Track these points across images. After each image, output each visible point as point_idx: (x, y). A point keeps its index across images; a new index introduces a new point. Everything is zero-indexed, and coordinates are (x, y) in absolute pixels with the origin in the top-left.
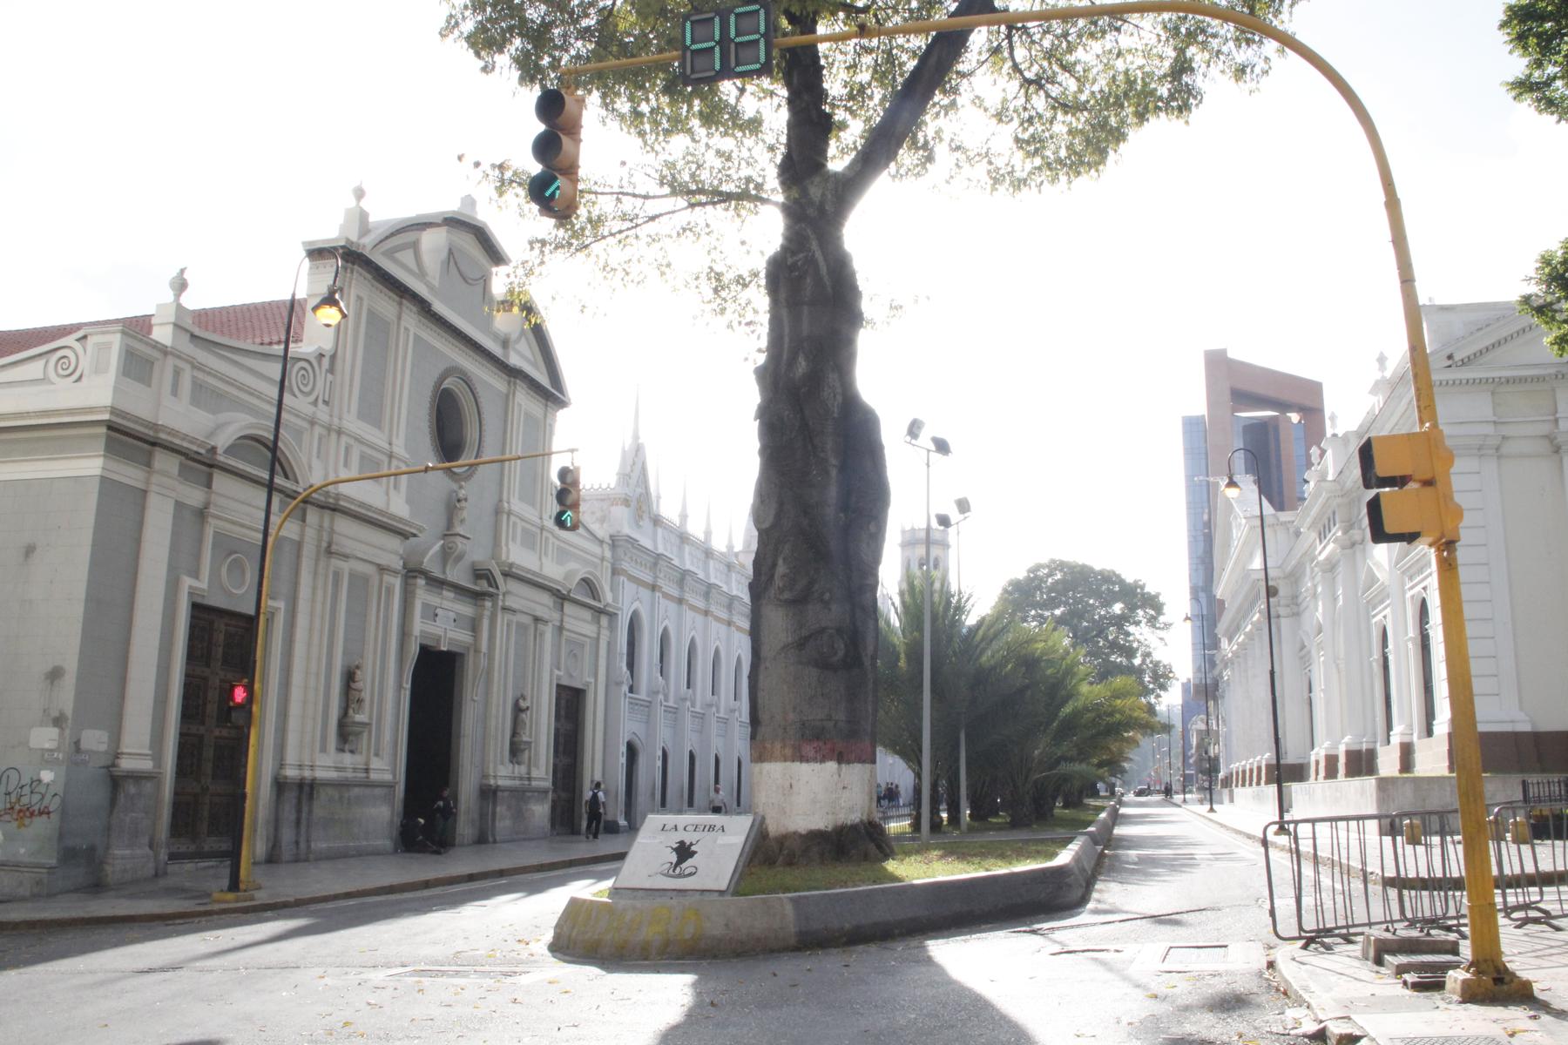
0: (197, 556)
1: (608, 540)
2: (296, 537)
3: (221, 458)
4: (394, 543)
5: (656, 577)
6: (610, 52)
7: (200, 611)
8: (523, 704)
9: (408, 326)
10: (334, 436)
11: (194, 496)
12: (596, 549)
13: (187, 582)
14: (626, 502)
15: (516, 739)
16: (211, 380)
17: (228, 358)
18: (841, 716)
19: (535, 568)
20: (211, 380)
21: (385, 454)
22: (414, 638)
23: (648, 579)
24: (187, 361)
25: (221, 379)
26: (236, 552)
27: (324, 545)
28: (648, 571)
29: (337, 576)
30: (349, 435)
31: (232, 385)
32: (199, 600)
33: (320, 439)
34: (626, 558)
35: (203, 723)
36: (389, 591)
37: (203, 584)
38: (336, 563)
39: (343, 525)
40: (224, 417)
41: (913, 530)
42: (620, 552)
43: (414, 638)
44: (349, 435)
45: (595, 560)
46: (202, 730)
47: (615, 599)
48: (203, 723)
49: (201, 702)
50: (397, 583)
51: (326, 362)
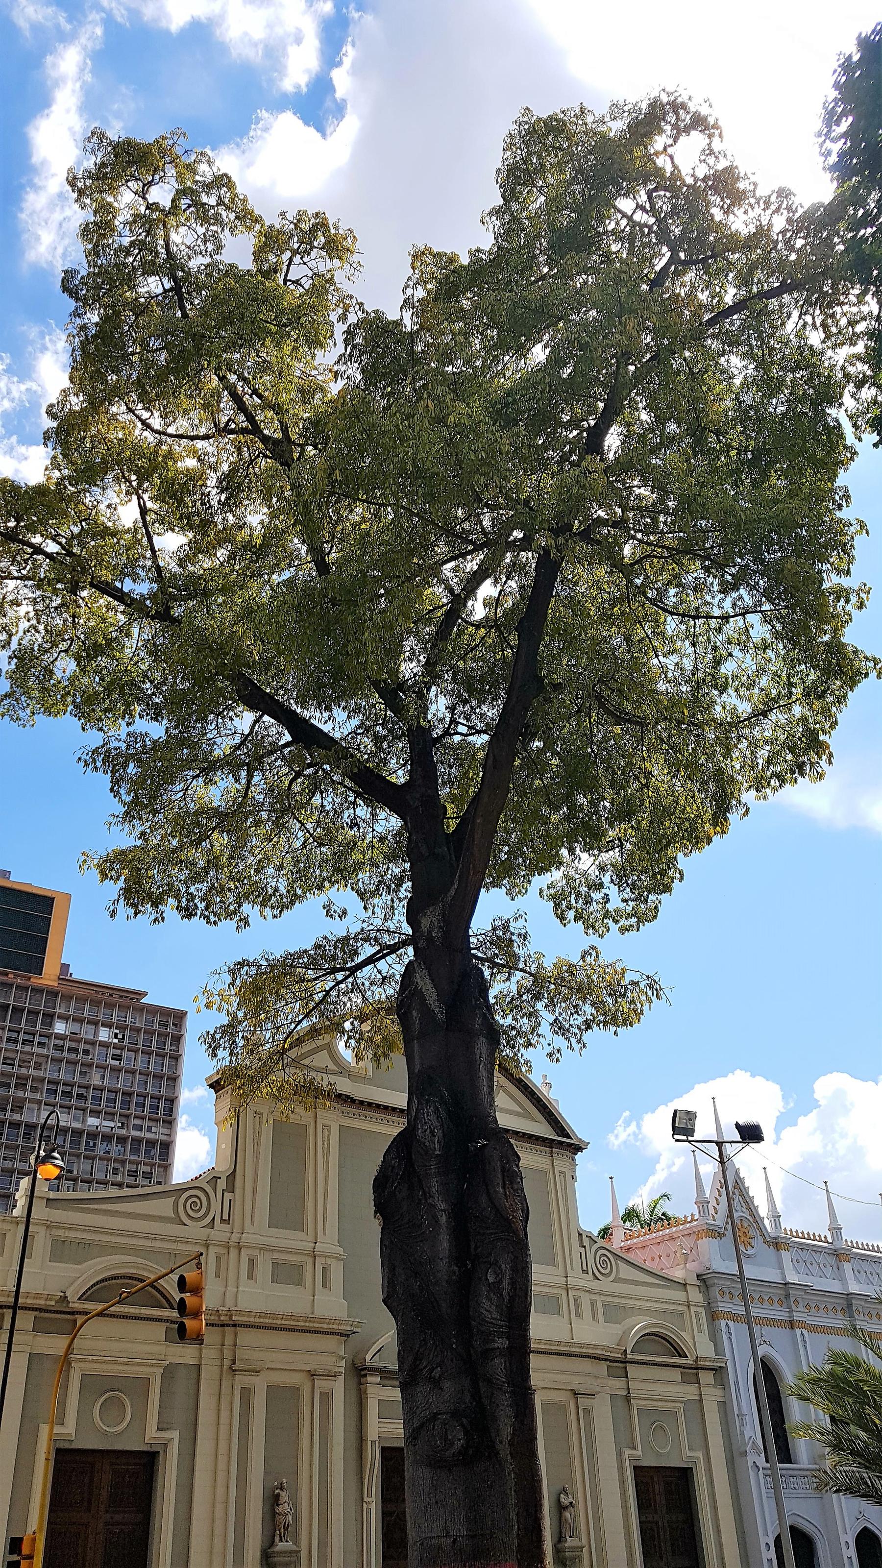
0: (63, 1404)
1: (693, 1280)
2: (193, 1362)
3: (76, 1305)
4: (331, 1343)
5: (791, 1311)
6: (155, 513)
7: (638, 1470)
8: (565, 1500)
9: (327, 1122)
10: (233, 1252)
11: (618, 1385)
12: (680, 1295)
13: (628, 1452)
14: (714, 1233)
15: (559, 1546)
16: (72, 1234)
17: (100, 1210)
18: (460, 1529)
19: (564, 1336)
20: (72, 1234)
21: (562, 1288)
22: (369, 1443)
23: (782, 1315)
24: (333, 1257)
25: (118, 1235)
26: (119, 1390)
27: (227, 1363)
28: (776, 1306)
29: (247, 1394)
30: (248, 1247)
31: (127, 1235)
32: (62, 1445)
33: (218, 1259)
34: (801, 1308)
35: (656, 1512)
36: (326, 1397)
37: (69, 1429)
38: (241, 1380)
39: (246, 1337)
40: (629, 1321)
41: (736, 167)
42: (715, 1292)
43: (369, 1443)
44: (248, 1247)
45: (680, 1308)
46: (656, 1517)
47: (719, 1350)
48: (656, 1512)
49: (651, 1496)
50: (338, 1388)
51: (222, 1184)
